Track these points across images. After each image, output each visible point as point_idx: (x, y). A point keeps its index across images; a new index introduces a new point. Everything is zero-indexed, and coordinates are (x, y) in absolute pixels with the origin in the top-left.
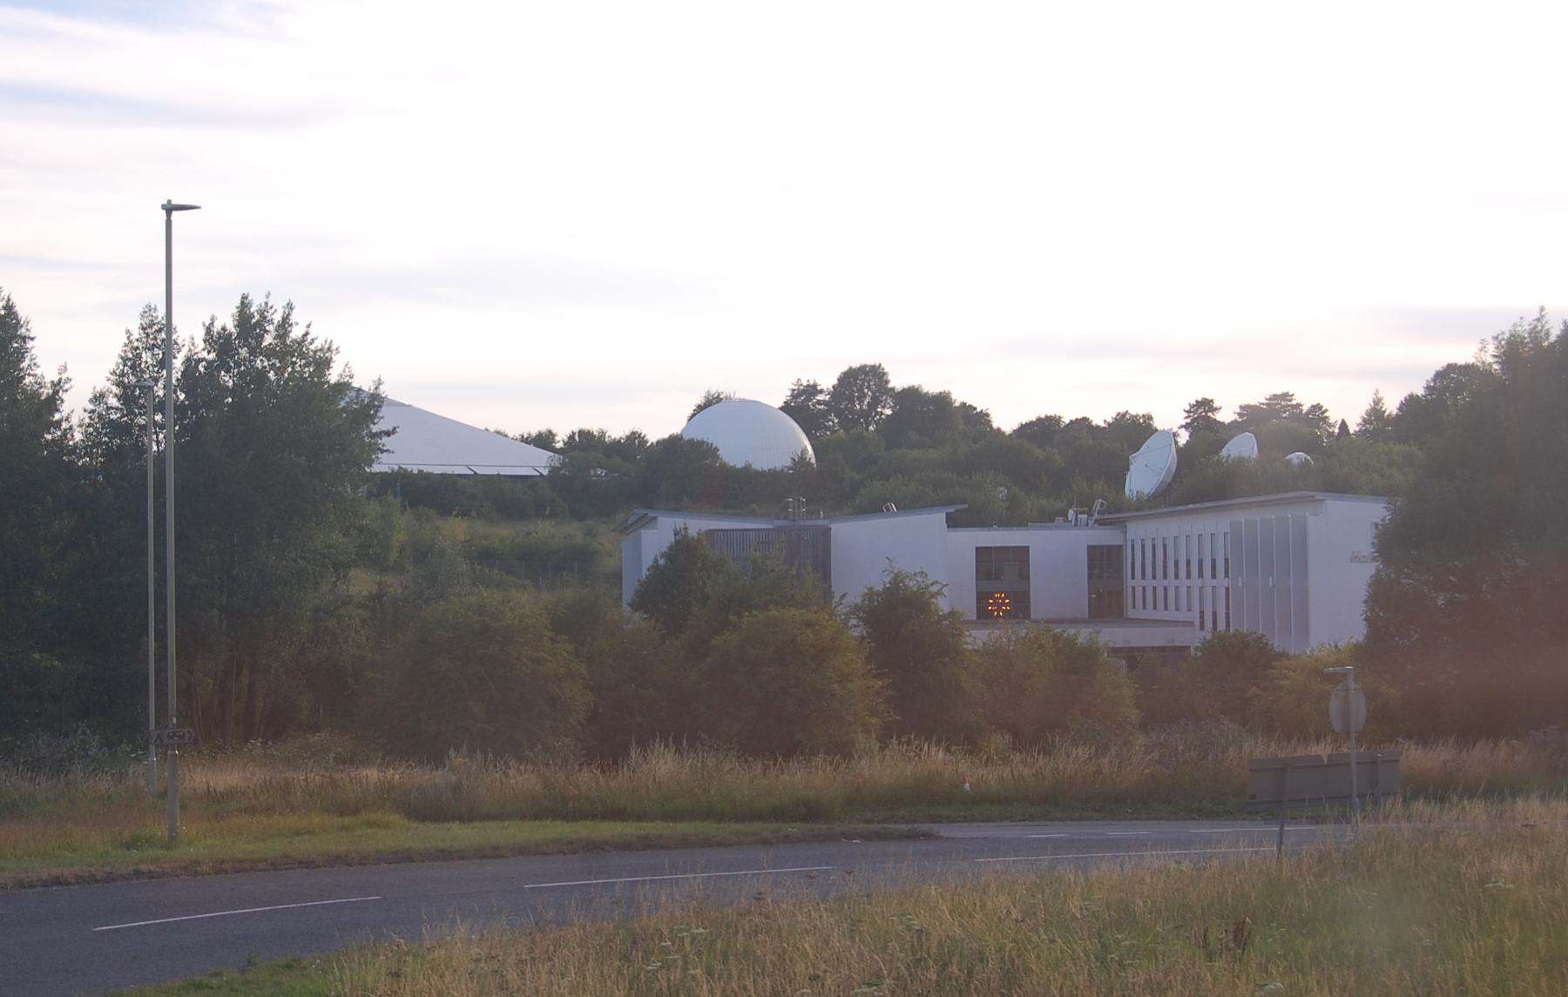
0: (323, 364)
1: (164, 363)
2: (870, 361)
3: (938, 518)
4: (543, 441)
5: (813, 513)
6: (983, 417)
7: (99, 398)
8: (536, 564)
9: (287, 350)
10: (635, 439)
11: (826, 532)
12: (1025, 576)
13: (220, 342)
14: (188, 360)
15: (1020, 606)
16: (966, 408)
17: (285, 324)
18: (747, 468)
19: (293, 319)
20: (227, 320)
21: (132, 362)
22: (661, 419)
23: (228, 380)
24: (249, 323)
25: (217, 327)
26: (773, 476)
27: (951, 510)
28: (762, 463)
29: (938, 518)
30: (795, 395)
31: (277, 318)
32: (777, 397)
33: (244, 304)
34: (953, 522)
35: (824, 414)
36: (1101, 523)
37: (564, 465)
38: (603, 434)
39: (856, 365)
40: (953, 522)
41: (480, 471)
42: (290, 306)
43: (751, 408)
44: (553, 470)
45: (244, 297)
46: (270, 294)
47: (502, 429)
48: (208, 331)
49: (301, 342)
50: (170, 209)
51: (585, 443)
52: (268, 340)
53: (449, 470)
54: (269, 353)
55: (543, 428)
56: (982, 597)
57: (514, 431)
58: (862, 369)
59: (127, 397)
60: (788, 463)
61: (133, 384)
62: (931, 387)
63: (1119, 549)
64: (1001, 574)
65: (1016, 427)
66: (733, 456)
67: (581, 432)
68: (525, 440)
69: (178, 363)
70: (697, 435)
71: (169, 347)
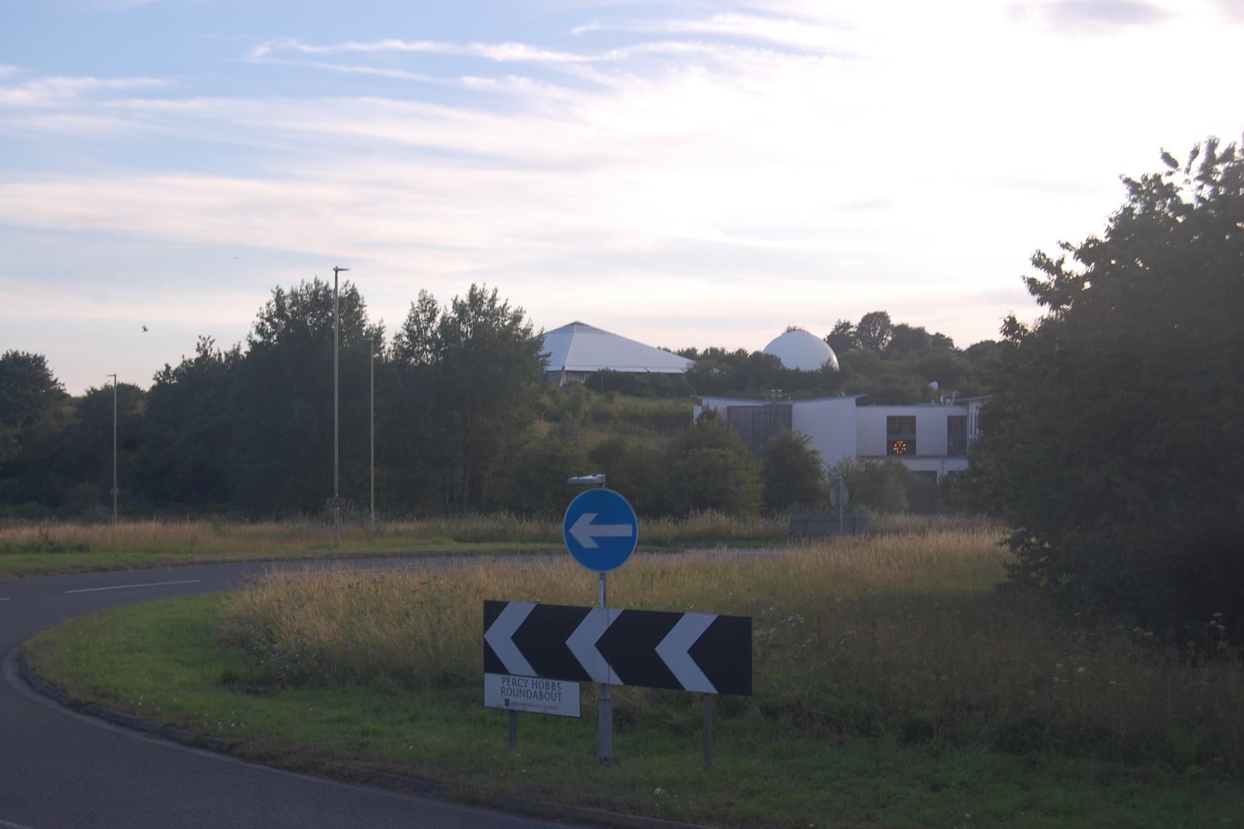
0: (517, 318)
1: (431, 319)
2: (880, 310)
3: (852, 401)
4: (690, 354)
5: (784, 398)
6: (949, 342)
7: (398, 337)
8: (659, 422)
9: (496, 313)
10: (741, 353)
11: (790, 408)
12: (913, 431)
13: (459, 308)
14: (443, 318)
15: (911, 450)
16: (939, 336)
17: (493, 300)
18: (797, 370)
19: (498, 296)
20: (464, 297)
21: (414, 319)
22: (754, 342)
23: (463, 328)
24: (475, 298)
25: (459, 300)
26: (811, 375)
27: (859, 396)
28: (805, 367)
29: (852, 401)
30: (837, 328)
31: (490, 296)
32: (822, 332)
33: (473, 288)
34: (859, 403)
35: (853, 339)
36: (956, 404)
37: (695, 367)
38: (723, 350)
39: (872, 311)
40: (859, 403)
41: (651, 370)
42: (496, 290)
43: (813, 339)
44: (690, 371)
45: (473, 286)
46: (487, 286)
47: (668, 347)
48: (455, 302)
49: (503, 308)
50: (337, 270)
51: (714, 355)
52: (485, 307)
53: (630, 370)
54: (485, 314)
55: (690, 346)
56: (890, 444)
57: (674, 349)
58: (875, 314)
59: (411, 334)
60: (819, 367)
61: (415, 330)
62: (914, 323)
63: (965, 418)
64: (900, 430)
65: (968, 346)
66: (789, 363)
67: (712, 349)
68: (680, 354)
69: (438, 319)
70: (770, 353)
71: (434, 313)
